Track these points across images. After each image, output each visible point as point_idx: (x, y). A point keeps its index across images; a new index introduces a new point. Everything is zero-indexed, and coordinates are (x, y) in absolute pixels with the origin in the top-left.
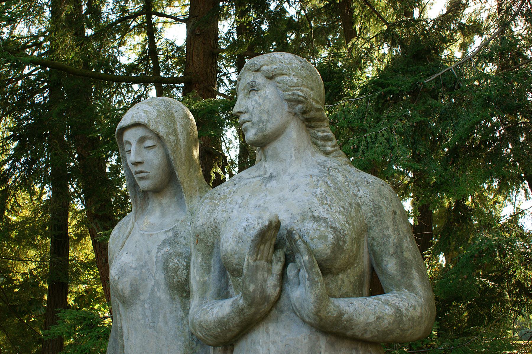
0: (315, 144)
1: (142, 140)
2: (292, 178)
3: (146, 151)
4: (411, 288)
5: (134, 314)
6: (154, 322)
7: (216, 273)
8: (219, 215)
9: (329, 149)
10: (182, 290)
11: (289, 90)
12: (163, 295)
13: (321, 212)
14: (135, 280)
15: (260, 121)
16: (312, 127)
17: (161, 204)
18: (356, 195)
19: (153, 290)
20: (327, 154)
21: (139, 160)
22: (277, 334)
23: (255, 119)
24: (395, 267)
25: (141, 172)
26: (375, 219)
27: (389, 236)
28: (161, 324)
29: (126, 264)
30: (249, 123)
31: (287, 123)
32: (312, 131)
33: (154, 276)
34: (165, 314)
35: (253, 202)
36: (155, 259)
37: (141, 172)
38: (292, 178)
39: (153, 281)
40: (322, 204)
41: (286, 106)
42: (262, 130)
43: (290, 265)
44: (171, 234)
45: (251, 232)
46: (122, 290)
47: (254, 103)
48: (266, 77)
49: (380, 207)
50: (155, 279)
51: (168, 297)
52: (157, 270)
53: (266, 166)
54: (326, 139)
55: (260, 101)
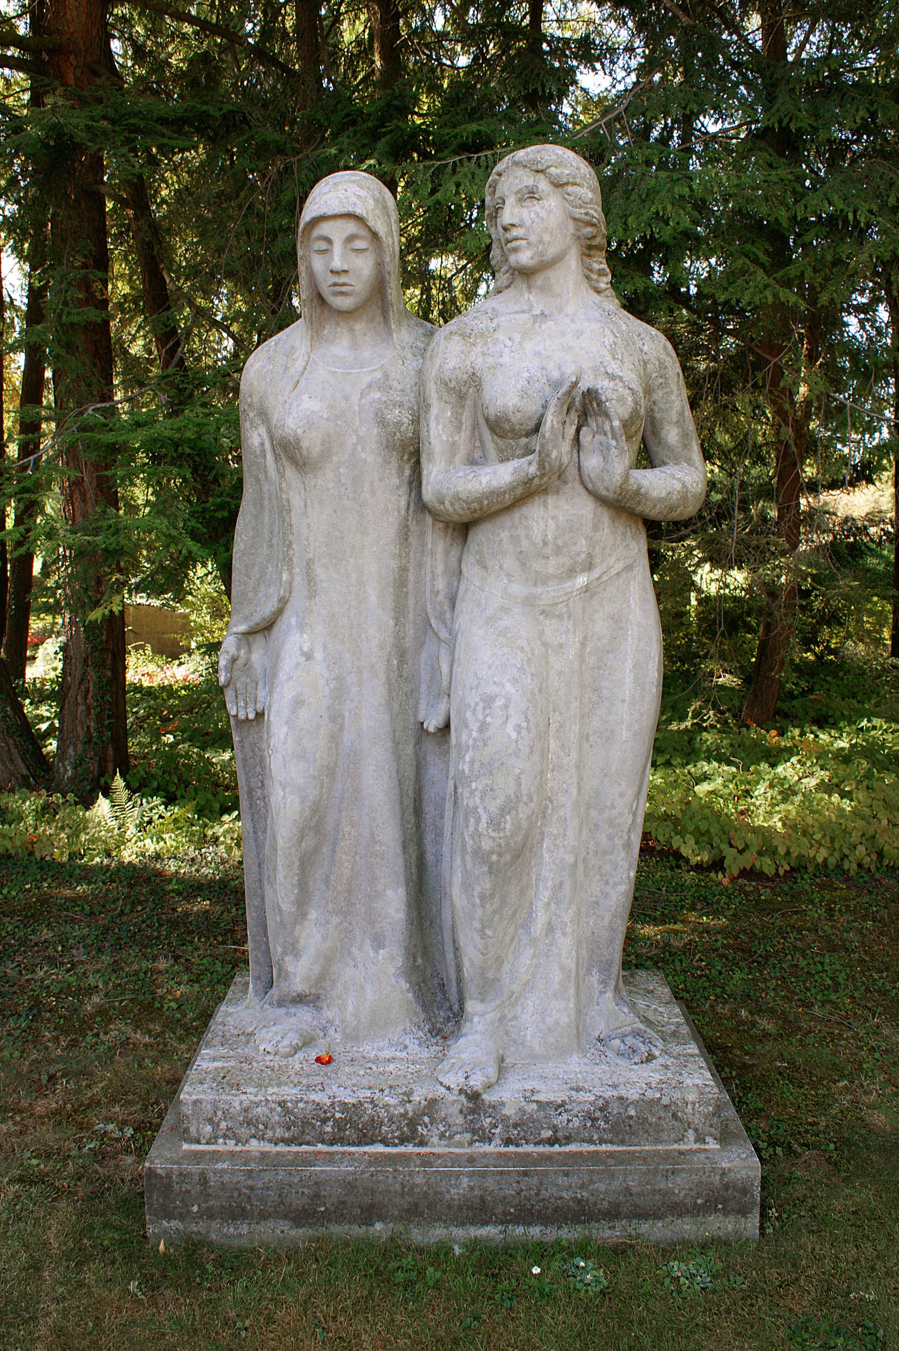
0: (588, 277)
1: (351, 239)
2: (573, 321)
3: (353, 255)
4: (689, 461)
5: (319, 482)
6: (355, 492)
7: (468, 432)
8: (477, 358)
9: (603, 286)
10: (411, 454)
11: (581, 207)
12: (371, 456)
13: (613, 367)
14: (329, 436)
15: (541, 242)
16: (589, 256)
17: (351, 330)
18: (642, 351)
19: (354, 450)
20: (598, 292)
21: (345, 267)
22: (557, 507)
23: (533, 238)
24: (676, 438)
25: (344, 284)
26: (660, 380)
27: (673, 402)
28: (366, 495)
29: (313, 412)
30: (524, 242)
31: (569, 247)
32: (587, 260)
33: (356, 432)
34: (373, 481)
35: (529, 346)
36: (356, 408)
37: (344, 284)
38: (573, 321)
39: (355, 437)
40: (614, 359)
41: (571, 226)
42: (541, 254)
43: (584, 430)
44: (378, 375)
45: (536, 385)
46: (308, 449)
47: (533, 215)
48: (552, 183)
49: (666, 368)
50: (358, 435)
51: (380, 460)
52: (361, 423)
53: (532, 298)
54: (601, 273)
55: (543, 214)
